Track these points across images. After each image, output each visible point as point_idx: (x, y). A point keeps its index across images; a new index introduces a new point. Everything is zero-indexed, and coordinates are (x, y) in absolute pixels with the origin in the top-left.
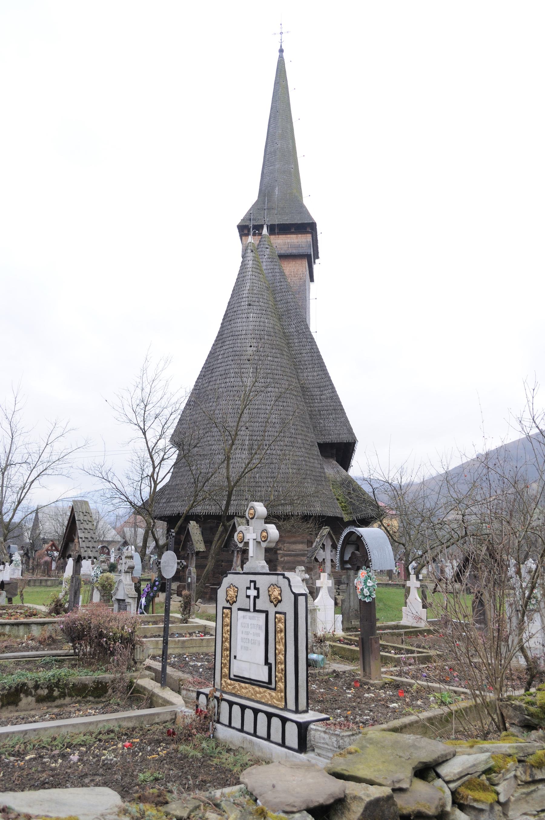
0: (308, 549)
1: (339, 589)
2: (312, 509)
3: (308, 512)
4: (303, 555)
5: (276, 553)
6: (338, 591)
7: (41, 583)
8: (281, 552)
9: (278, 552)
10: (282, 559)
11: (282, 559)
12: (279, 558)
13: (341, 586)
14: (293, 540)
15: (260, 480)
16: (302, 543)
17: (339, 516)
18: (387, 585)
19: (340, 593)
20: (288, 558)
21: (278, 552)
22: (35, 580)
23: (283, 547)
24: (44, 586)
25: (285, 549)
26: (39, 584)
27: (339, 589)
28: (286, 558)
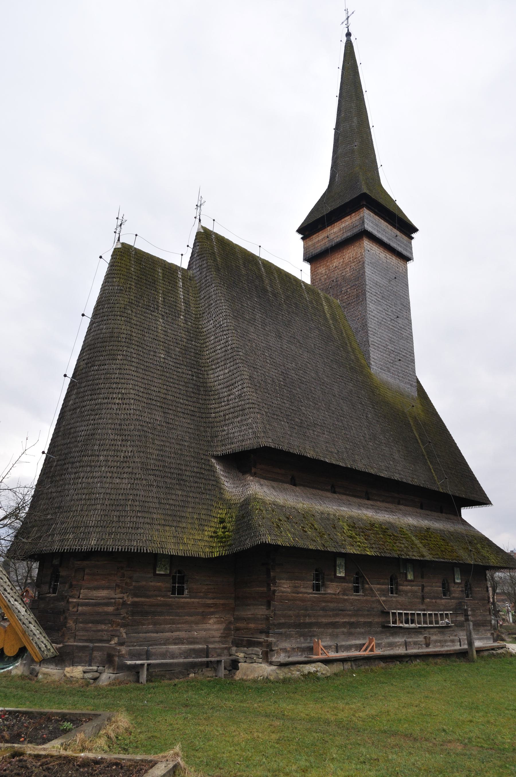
4: (107, 604)
8: (75, 600)
12: (71, 609)
14: (95, 583)
16: (108, 588)
20: (84, 608)
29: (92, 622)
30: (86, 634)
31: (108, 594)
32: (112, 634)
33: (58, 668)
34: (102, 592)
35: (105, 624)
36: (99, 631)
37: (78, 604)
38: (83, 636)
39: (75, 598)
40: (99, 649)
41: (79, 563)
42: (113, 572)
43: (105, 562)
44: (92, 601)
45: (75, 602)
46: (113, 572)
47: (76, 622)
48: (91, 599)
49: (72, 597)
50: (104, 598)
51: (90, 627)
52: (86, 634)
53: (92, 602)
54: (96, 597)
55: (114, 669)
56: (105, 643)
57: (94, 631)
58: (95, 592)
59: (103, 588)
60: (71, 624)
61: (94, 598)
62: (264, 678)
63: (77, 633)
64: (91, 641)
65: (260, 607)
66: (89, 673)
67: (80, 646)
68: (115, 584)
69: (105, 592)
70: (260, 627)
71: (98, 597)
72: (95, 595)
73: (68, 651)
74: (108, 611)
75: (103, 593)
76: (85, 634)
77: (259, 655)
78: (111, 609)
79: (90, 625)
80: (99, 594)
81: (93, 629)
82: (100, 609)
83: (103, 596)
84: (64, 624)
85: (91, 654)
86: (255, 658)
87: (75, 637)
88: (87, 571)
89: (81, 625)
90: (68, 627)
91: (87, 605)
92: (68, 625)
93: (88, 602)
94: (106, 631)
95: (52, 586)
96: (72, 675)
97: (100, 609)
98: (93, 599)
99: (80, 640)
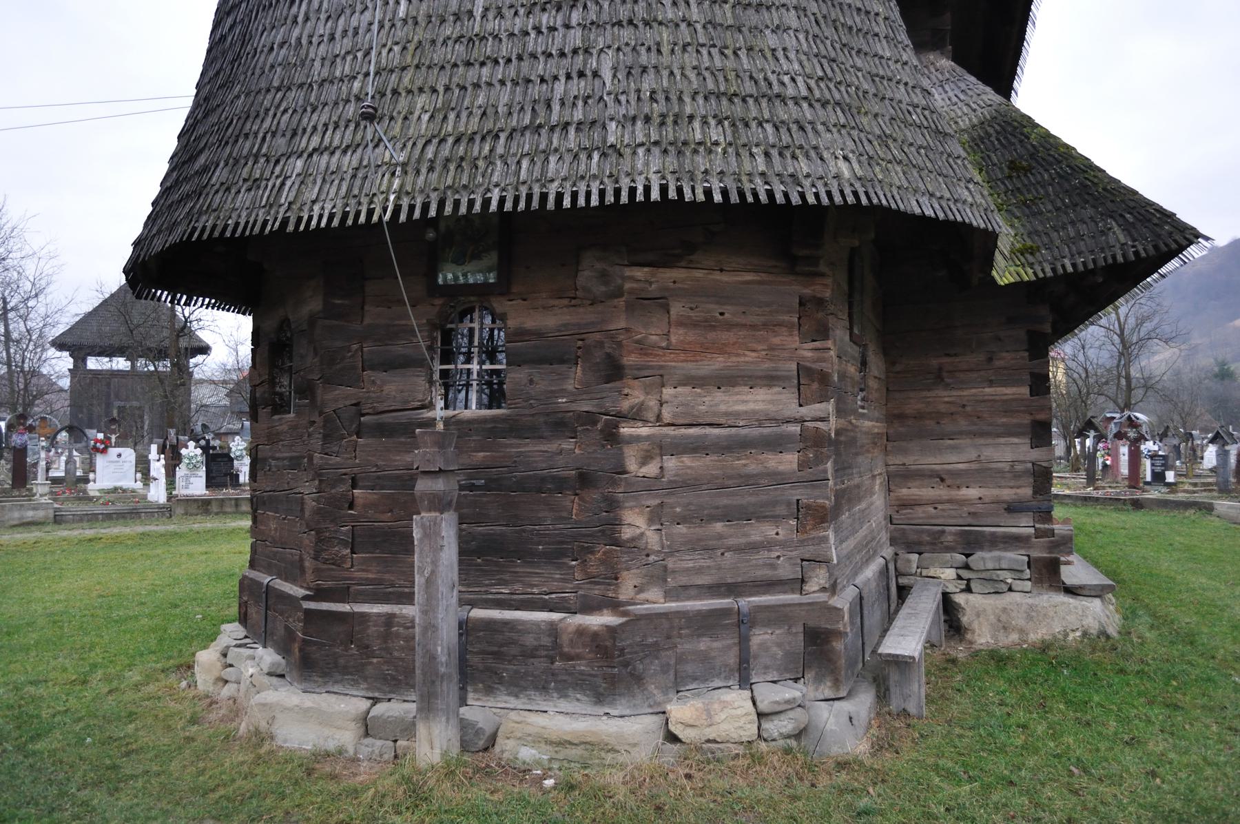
0: (805, 411)
1: (967, 567)
2: (804, 166)
3: (779, 190)
4: (776, 444)
5: (611, 437)
6: (965, 574)
7: (237, 505)
8: (644, 431)
9: (626, 430)
10: (651, 469)
11: (651, 469)
12: (632, 465)
13: (979, 554)
14: (715, 364)
15: (492, 25)
16: (770, 380)
17: (978, 222)
18: (1086, 499)
19: (973, 585)
20: (687, 460)
21: (626, 430)
22: (223, 500)
23: (652, 403)
24: (217, 514)
25: (667, 415)
26: (233, 509)
27: (967, 567)
28: (671, 463)
29: (727, 516)
30: (709, 562)
31: (771, 402)
32: (807, 556)
33: (613, 712)
34: (749, 397)
35: (776, 519)
36: (755, 547)
37: (662, 448)
38: (699, 571)
39: (645, 421)
40: (776, 616)
41: (640, 273)
42: (786, 318)
43: (749, 277)
44: (716, 431)
45: (648, 438)
46: (786, 318)
47: (656, 516)
48: (711, 425)
49: (636, 415)
50: (761, 420)
51: (720, 537)
52: (709, 562)
53: (718, 437)
54: (727, 414)
55: (837, 683)
56: (785, 592)
57: (739, 549)
58: (719, 396)
59: (753, 380)
60: (635, 523)
61: (722, 421)
62: (1085, 634)
63: (670, 563)
64: (733, 589)
65: (1002, 440)
66: (782, 717)
67: (699, 613)
68: (794, 366)
69: (759, 397)
70: (1007, 494)
71: (737, 415)
72: (723, 408)
73: (650, 640)
74: (781, 468)
75: (757, 400)
76: (702, 563)
77: (1022, 571)
78: (788, 461)
79: (719, 527)
80: (737, 402)
81: (731, 542)
82: (749, 464)
83: (754, 412)
84: (609, 530)
85: (744, 642)
86: (1009, 581)
87: (659, 576)
88: (677, 309)
89: (682, 529)
90: (633, 539)
91: (696, 448)
92: (627, 533)
93: (699, 436)
94: (784, 545)
95: (436, 376)
96: (711, 733)
97: (749, 464)
98: (719, 425)
99: (683, 591)
